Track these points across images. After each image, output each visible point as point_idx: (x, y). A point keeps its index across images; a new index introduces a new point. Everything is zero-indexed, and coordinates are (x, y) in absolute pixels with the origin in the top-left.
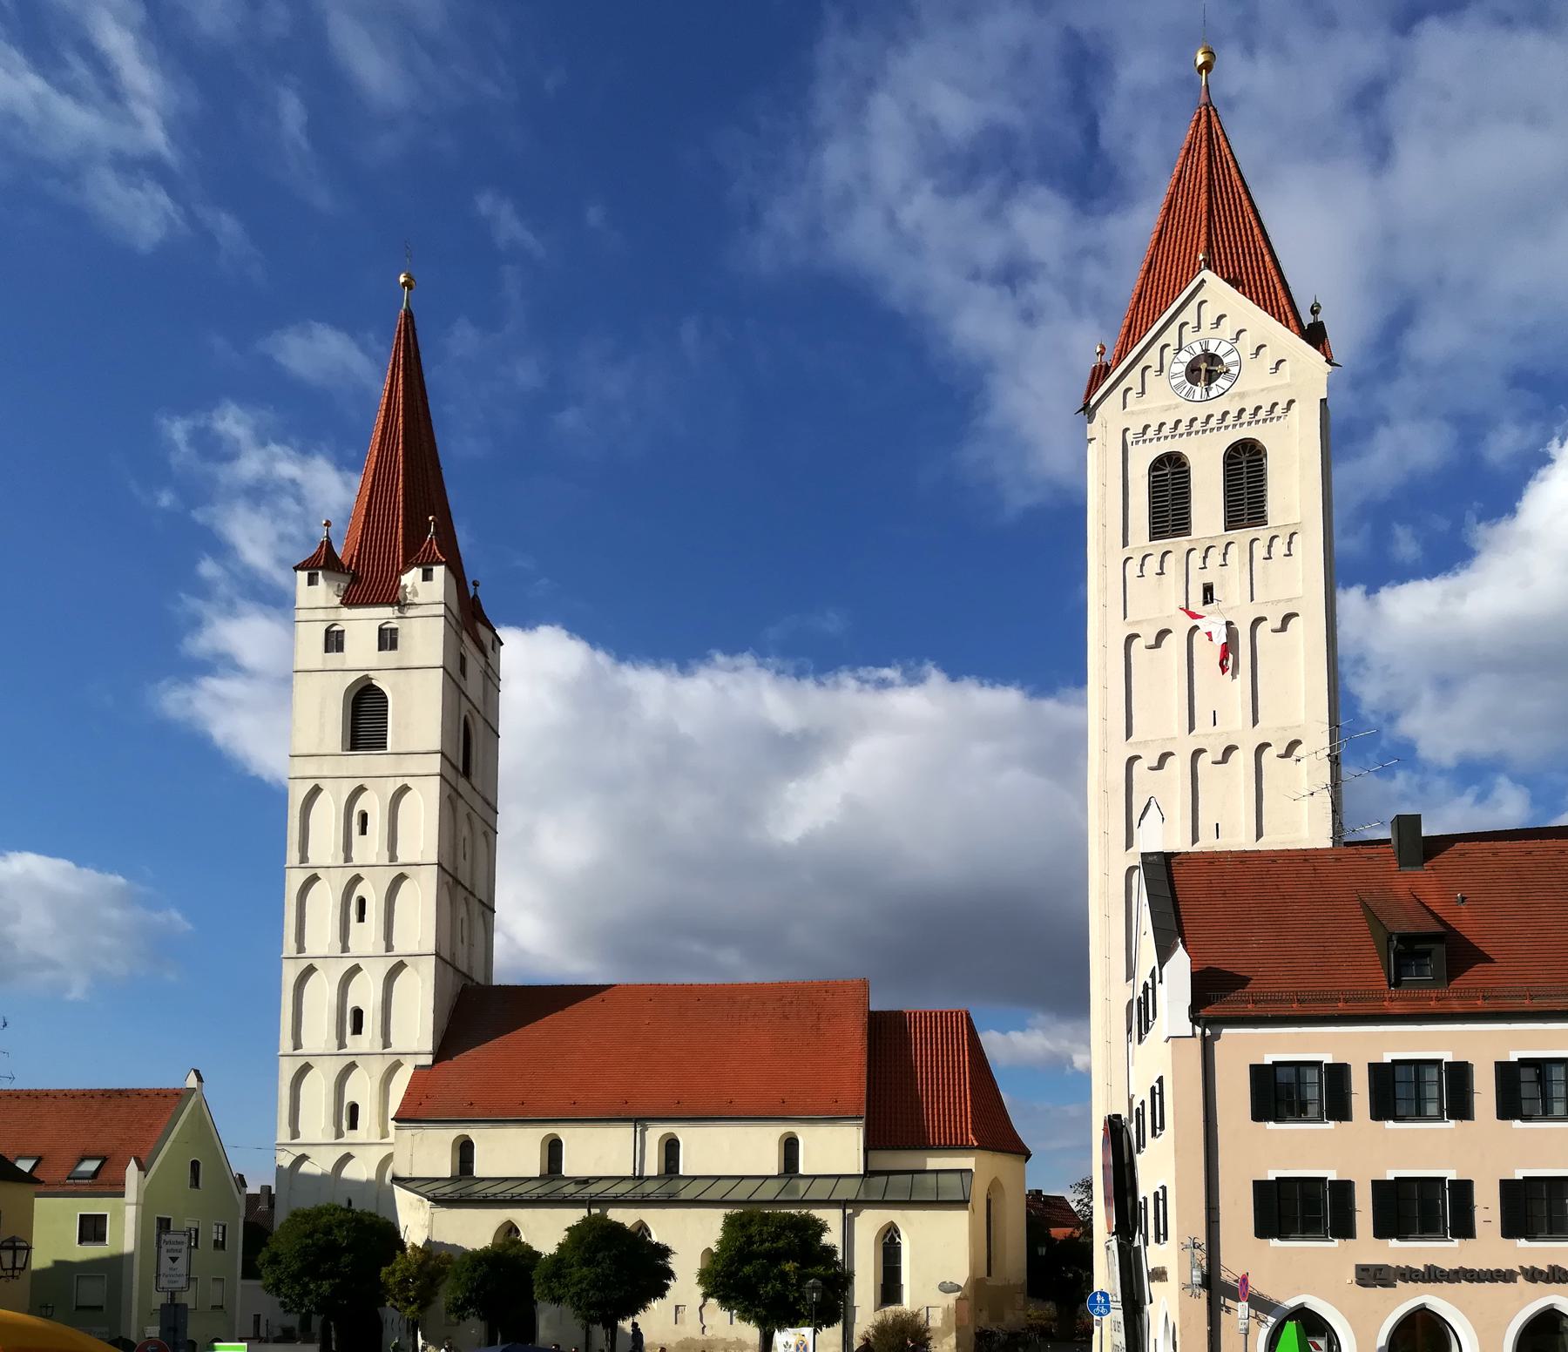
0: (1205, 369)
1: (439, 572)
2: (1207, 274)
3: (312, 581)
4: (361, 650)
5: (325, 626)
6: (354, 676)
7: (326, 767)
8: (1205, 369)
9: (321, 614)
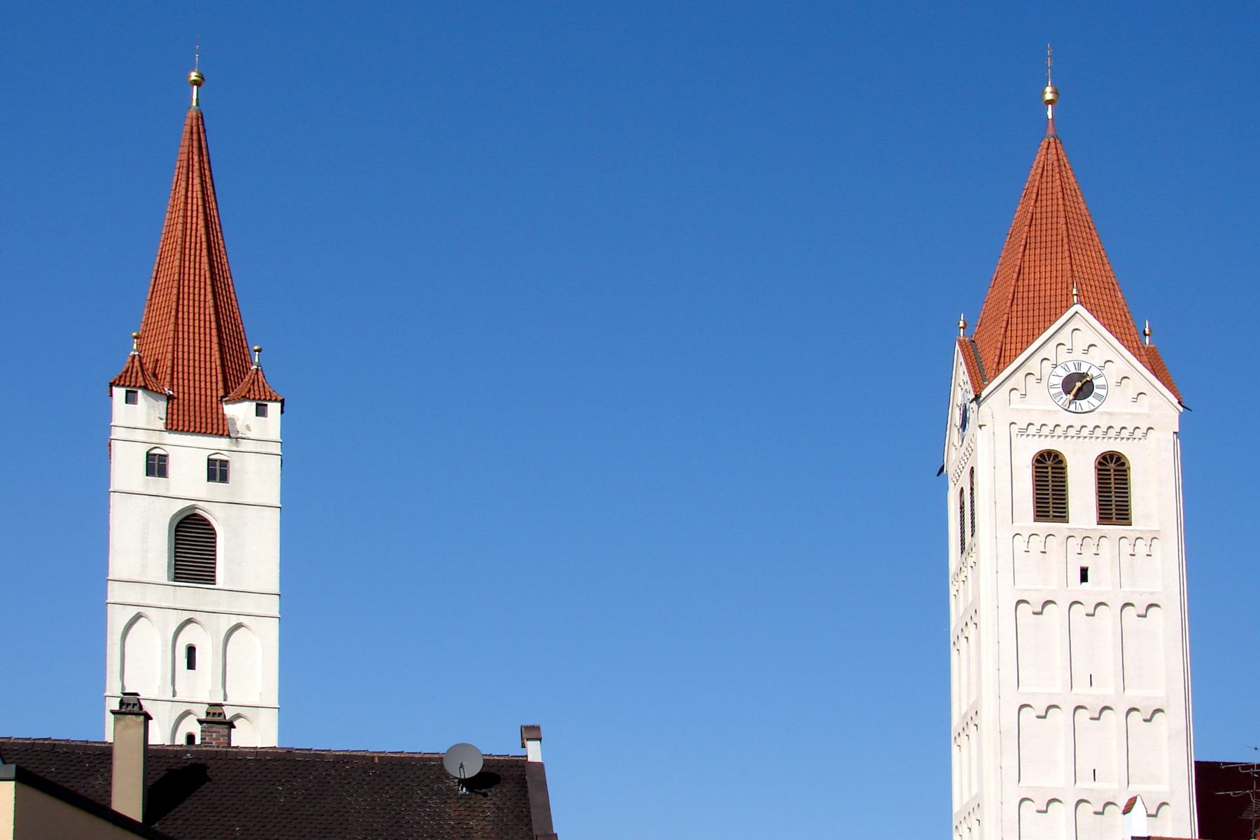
0: (1079, 386)
1: (274, 408)
2: (1078, 308)
3: (130, 398)
4: (188, 479)
5: (147, 447)
6: (180, 505)
7: (151, 596)
8: (1079, 386)
9: (140, 435)
